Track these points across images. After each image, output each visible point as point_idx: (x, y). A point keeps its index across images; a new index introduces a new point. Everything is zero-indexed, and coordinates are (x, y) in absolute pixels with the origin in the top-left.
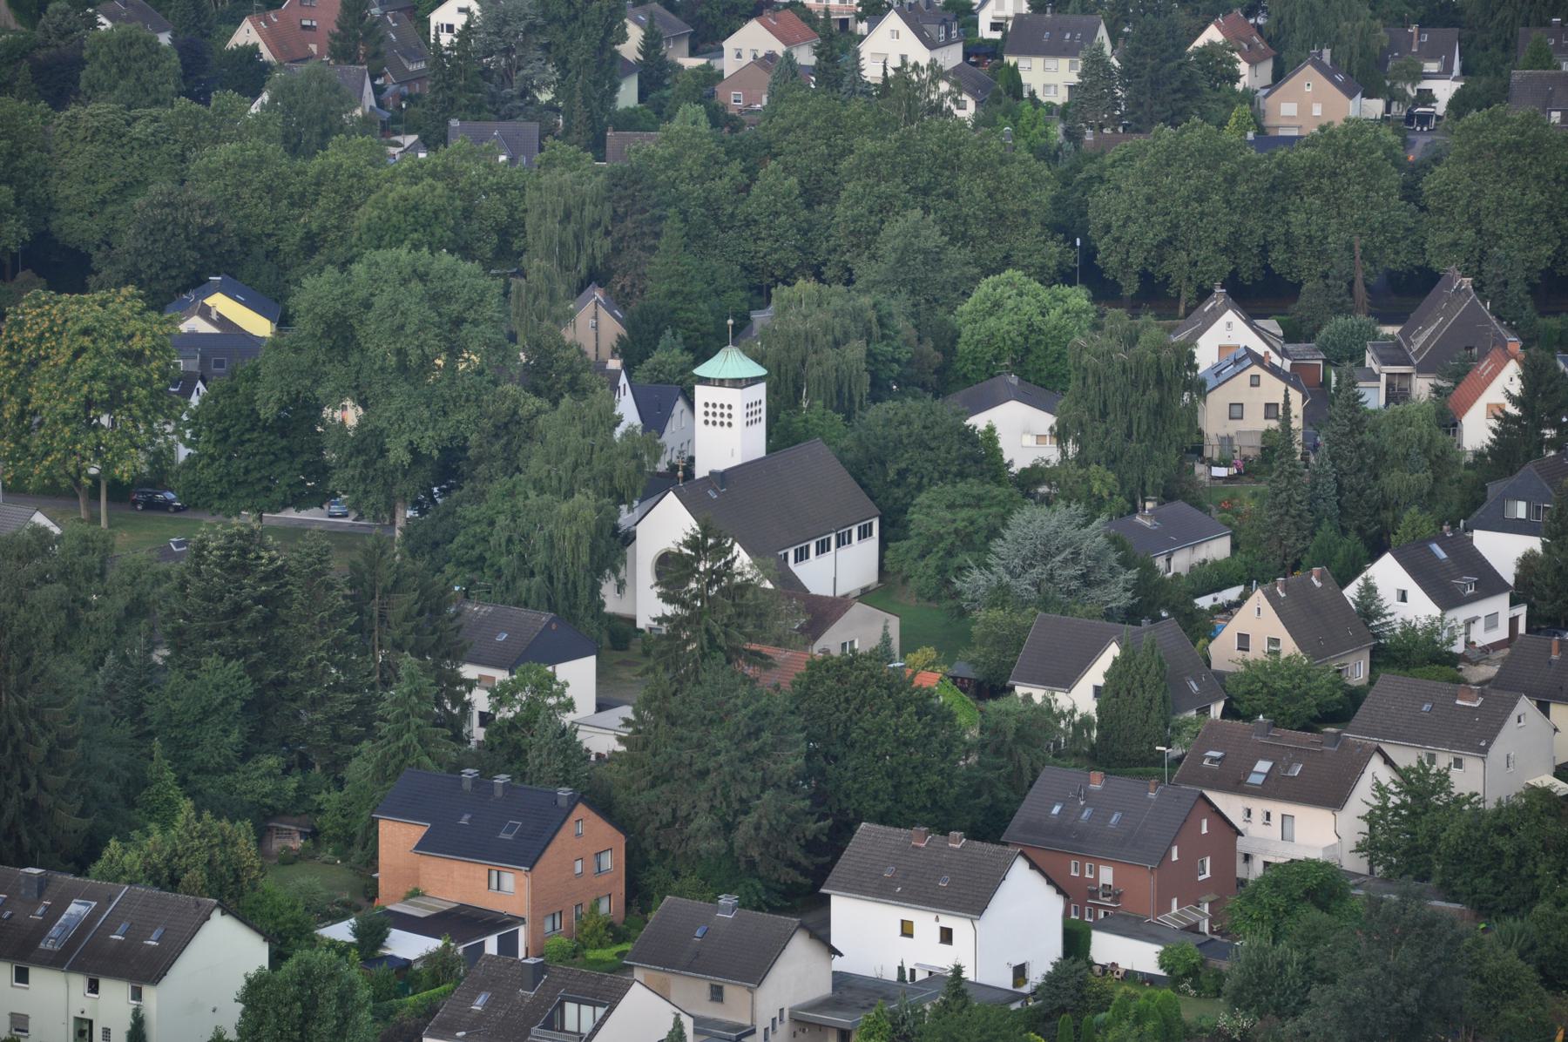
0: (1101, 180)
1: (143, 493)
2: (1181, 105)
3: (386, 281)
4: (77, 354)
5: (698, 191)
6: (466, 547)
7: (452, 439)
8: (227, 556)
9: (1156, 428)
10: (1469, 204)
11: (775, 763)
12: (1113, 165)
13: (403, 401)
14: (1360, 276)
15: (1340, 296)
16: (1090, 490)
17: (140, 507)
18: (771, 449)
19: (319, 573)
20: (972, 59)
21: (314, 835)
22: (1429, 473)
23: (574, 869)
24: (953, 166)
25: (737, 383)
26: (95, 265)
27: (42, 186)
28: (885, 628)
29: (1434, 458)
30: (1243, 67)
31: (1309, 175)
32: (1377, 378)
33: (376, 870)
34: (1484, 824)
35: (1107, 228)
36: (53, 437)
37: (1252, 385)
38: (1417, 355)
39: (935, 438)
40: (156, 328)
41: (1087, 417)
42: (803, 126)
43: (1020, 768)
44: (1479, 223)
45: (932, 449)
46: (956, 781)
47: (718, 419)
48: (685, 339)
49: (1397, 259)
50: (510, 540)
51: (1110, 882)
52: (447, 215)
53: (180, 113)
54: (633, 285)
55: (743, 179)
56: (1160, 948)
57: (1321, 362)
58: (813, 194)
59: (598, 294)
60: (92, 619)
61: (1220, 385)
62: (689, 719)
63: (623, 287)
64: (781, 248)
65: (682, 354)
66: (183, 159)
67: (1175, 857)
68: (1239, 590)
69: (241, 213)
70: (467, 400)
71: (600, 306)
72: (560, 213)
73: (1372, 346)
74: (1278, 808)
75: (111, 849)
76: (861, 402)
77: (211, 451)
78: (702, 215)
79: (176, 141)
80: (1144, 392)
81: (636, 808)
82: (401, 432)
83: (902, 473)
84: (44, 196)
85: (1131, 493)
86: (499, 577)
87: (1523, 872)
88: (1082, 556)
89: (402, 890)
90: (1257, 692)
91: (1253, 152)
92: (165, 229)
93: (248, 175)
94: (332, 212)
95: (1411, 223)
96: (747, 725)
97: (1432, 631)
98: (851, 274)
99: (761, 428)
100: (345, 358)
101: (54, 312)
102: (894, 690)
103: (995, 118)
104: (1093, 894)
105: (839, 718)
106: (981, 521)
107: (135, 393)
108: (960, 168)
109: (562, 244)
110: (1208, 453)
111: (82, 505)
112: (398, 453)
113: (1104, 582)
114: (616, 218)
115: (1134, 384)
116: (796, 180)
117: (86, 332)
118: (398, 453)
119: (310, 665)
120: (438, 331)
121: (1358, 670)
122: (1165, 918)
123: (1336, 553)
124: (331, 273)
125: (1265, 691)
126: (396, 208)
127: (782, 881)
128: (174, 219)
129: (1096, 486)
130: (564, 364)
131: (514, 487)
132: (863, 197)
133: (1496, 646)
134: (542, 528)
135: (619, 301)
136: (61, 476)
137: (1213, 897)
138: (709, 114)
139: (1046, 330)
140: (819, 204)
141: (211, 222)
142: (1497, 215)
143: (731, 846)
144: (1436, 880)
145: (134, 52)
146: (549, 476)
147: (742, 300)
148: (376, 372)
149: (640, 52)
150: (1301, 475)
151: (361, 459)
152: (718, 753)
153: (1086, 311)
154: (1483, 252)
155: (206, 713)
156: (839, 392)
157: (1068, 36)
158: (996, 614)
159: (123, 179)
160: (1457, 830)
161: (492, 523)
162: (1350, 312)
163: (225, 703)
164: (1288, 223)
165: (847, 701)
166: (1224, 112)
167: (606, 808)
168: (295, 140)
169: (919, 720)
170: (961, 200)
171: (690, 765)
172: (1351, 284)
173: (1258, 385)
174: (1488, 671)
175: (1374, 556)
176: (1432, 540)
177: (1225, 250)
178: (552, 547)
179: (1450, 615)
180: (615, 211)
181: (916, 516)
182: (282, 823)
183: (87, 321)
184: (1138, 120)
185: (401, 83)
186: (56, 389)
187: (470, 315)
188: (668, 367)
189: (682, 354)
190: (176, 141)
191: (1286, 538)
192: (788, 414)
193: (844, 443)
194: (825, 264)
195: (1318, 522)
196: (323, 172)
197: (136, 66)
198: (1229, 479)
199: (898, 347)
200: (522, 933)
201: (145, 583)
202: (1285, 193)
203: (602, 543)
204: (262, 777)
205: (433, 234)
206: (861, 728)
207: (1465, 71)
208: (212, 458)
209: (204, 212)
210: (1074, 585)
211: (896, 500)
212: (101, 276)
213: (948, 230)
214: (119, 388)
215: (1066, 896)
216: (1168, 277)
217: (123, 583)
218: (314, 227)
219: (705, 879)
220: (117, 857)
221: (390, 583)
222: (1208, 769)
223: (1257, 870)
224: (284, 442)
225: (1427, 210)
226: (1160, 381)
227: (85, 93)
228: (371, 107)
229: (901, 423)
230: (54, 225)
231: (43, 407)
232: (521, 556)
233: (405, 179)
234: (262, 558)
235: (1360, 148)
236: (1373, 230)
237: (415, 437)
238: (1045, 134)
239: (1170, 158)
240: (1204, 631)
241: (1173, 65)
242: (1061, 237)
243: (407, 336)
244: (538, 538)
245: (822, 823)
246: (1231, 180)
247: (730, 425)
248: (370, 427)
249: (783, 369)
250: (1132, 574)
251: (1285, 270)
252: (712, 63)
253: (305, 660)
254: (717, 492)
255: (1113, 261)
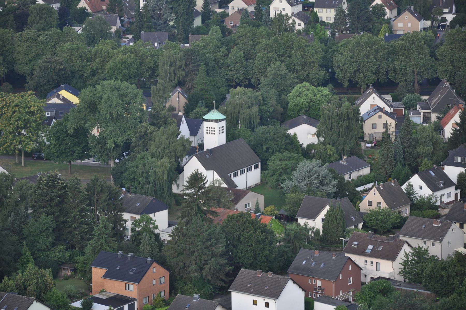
0: (337, 51)
1: (37, 154)
2: (366, 24)
3: (107, 91)
4: (14, 112)
5: (212, 56)
6: (129, 175)
7: (127, 140)
8: (48, 183)
9: (347, 133)
10: (450, 58)
11: (216, 249)
12: (341, 47)
13: (112, 128)
14: (416, 81)
15: (410, 87)
16: (327, 153)
17: (35, 159)
18: (227, 141)
19: (77, 188)
20: (306, 8)
21: (75, 270)
22: (432, 147)
23: (152, 283)
24: (290, 48)
25: (217, 121)
26: (27, 80)
27: (11, 56)
28: (257, 200)
29: (433, 142)
30: (387, 11)
31: (401, 49)
32: (420, 114)
33: (91, 283)
34: (438, 267)
35: (339, 66)
36: (6, 138)
37: (379, 118)
38: (432, 107)
39: (278, 137)
40: (38, 104)
41: (326, 129)
42: (245, 35)
43: (296, 247)
44: (454, 64)
45: (277, 141)
46: (274, 253)
47: (211, 132)
48: (206, 104)
49: (427, 76)
50: (143, 173)
51: (320, 285)
52: (135, 64)
53: (54, 33)
54: (192, 86)
55: (226, 52)
56: (335, 307)
57: (403, 108)
58: (248, 57)
59: (179, 90)
60: (7, 202)
61: (369, 118)
62: (189, 235)
63: (189, 86)
64: (238, 73)
65: (204, 108)
66: (55, 47)
67: (341, 278)
68: (372, 184)
69: (72, 64)
70: (132, 128)
71: (180, 93)
72: (169, 64)
73: (419, 103)
74: (375, 260)
75: (5, 280)
76: (257, 125)
77: (54, 143)
78: (213, 63)
79: (53, 42)
80: (344, 122)
81: (172, 263)
82: (111, 138)
83: (267, 149)
84: (12, 59)
85: (340, 153)
86: (139, 184)
87: (450, 282)
88: (320, 176)
89: (99, 289)
90: (373, 220)
91: (384, 43)
92: (48, 69)
93: (74, 52)
94: (100, 63)
95: (433, 64)
96: (207, 237)
97: (430, 199)
98: (260, 82)
99: (224, 135)
100: (95, 115)
101: (7, 99)
102: (254, 224)
103: (309, 29)
104: (316, 289)
105: (237, 234)
106: (290, 165)
107: (32, 124)
108: (293, 48)
109: (170, 73)
110: (365, 139)
111: (17, 159)
112: (110, 144)
113: (328, 184)
114: (186, 65)
115: (340, 119)
116: (242, 52)
117: (16, 106)
118: (110, 144)
119: (74, 216)
120: (122, 106)
121: (406, 212)
122: (338, 297)
123: (402, 173)
124: (89, 88)
125: (375, 219)
126: (119, 62)
127: (218, 285)
128: (51, 67)
129: (329, 151)
130: (162, 116)
131: (144, 156)
132: (263, 57)
133: (450, 203)
134: (152, 169)
135: (186, 91)
136: (9, 150)
137: (353, 290)
138: (221, 29)
139: (315, 101)
140: (250, 59)
141: (62, 67)
142: (459, 61)
143: (202, 275)
144: (423, 284)
145: (44, 12)
146: (156, 151)
147: (225, 90)
148: (103, 119)
149: (202, 8)
150: (391, 148)
151: (100, 146)
152: (197, 246)
153: (328, 95)
154: (455, 73)
155: (41, 232)
156: (250, 122)
157: (334, 2)
158: (293, 195)
159: (36, 53)
160: (429, 269)
161: (137, 167)
162: (413, 92)
163: (47, 229)
164: (395, 64)
165: (239, 228)
166: (380, 26)
167: (163, 263)
168: (92, 39)
169: (262, 234)
170: (293, 58)
171: (189, 249)
172: (414, 83)
173: (381, 118)
174: (446, 211)
175: (413, 175)
176: (430, 170)
177: (375, 73)
178: (156, 174)
179: (436, 194)
180: (186, 63)
181: (269, 163)
182: (65, 266)
183: (17, 102)
184: (353, 29)
185: (130, 19)
186: (7, 123)
187: (132, 101)
188: (200, 113)
189: (204, 108)
190: (53, 42)
191: (387, 168)
192: (233, 130)
193: (250, 139)
194: (251, 78)
195: (397, 163)
196: (97, 51)
197: (44, 16)
198: (372, 147)
199: (269, 107)
200: (136, 303)
201: (25, 190)
202: (394, 55)
203: (171, 173)
204: (59, 252)
205: (130, 70)
206: (244, 237)
207: (456, 11)
208: (55, 145)
209: (60, 64)
210: (318, 185)
211: (266, 156)
212: (29, 84)
213: (289, 67)
214: (27, 123)
215: (305, 291)
216: (357, 81)
217: (18, 190)
218: (94, 68)
219: (194, 285)
220: (6, 282)
221: (99, 190)
222: (353, 248)
223: (368, 280)
224: (77, 140)
225: (438, 60)
226: (348, 118)
227: (29, 25)
228: (119, 27)
229: (267, 133)
230: (15, 68)
231: (3, 129)
232: (146, 177)
233: (122, 53)
234: (59, 183)
235: (417, 41)
236: (421, 66)
237: (115, 139)
238: (324, 34)
239: (358, 44)
240: (359, 198)
241: (364, 12)
242: (324, 69)
243: (113, 108)
244: (151, 172)
245: (230, 268)
246: (377, 51)
247: (214, 134)
248: (102, 136)
249: (233, 115)
250: (336, 182)
251: (394, 79)
252: (225, 11)
253: (72, 215)
254: (209, 156)
255: (340, 76)
